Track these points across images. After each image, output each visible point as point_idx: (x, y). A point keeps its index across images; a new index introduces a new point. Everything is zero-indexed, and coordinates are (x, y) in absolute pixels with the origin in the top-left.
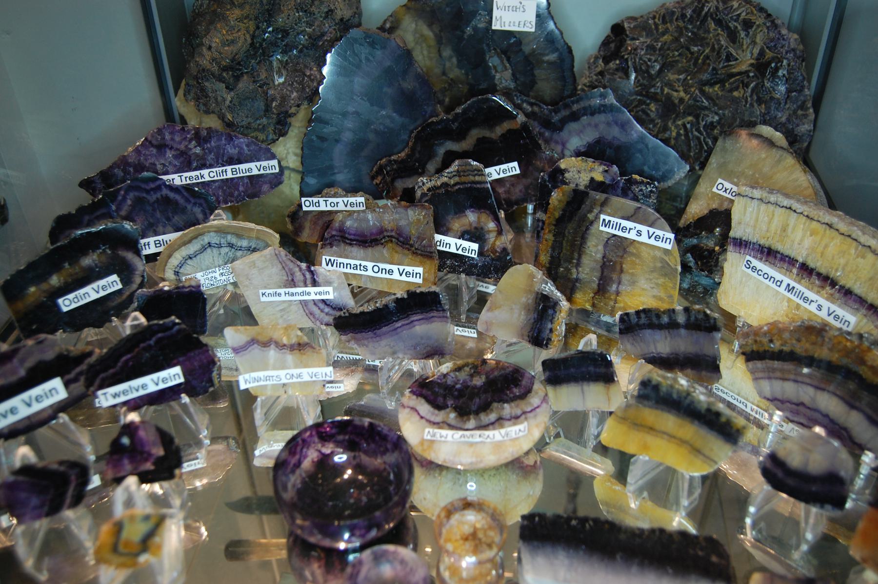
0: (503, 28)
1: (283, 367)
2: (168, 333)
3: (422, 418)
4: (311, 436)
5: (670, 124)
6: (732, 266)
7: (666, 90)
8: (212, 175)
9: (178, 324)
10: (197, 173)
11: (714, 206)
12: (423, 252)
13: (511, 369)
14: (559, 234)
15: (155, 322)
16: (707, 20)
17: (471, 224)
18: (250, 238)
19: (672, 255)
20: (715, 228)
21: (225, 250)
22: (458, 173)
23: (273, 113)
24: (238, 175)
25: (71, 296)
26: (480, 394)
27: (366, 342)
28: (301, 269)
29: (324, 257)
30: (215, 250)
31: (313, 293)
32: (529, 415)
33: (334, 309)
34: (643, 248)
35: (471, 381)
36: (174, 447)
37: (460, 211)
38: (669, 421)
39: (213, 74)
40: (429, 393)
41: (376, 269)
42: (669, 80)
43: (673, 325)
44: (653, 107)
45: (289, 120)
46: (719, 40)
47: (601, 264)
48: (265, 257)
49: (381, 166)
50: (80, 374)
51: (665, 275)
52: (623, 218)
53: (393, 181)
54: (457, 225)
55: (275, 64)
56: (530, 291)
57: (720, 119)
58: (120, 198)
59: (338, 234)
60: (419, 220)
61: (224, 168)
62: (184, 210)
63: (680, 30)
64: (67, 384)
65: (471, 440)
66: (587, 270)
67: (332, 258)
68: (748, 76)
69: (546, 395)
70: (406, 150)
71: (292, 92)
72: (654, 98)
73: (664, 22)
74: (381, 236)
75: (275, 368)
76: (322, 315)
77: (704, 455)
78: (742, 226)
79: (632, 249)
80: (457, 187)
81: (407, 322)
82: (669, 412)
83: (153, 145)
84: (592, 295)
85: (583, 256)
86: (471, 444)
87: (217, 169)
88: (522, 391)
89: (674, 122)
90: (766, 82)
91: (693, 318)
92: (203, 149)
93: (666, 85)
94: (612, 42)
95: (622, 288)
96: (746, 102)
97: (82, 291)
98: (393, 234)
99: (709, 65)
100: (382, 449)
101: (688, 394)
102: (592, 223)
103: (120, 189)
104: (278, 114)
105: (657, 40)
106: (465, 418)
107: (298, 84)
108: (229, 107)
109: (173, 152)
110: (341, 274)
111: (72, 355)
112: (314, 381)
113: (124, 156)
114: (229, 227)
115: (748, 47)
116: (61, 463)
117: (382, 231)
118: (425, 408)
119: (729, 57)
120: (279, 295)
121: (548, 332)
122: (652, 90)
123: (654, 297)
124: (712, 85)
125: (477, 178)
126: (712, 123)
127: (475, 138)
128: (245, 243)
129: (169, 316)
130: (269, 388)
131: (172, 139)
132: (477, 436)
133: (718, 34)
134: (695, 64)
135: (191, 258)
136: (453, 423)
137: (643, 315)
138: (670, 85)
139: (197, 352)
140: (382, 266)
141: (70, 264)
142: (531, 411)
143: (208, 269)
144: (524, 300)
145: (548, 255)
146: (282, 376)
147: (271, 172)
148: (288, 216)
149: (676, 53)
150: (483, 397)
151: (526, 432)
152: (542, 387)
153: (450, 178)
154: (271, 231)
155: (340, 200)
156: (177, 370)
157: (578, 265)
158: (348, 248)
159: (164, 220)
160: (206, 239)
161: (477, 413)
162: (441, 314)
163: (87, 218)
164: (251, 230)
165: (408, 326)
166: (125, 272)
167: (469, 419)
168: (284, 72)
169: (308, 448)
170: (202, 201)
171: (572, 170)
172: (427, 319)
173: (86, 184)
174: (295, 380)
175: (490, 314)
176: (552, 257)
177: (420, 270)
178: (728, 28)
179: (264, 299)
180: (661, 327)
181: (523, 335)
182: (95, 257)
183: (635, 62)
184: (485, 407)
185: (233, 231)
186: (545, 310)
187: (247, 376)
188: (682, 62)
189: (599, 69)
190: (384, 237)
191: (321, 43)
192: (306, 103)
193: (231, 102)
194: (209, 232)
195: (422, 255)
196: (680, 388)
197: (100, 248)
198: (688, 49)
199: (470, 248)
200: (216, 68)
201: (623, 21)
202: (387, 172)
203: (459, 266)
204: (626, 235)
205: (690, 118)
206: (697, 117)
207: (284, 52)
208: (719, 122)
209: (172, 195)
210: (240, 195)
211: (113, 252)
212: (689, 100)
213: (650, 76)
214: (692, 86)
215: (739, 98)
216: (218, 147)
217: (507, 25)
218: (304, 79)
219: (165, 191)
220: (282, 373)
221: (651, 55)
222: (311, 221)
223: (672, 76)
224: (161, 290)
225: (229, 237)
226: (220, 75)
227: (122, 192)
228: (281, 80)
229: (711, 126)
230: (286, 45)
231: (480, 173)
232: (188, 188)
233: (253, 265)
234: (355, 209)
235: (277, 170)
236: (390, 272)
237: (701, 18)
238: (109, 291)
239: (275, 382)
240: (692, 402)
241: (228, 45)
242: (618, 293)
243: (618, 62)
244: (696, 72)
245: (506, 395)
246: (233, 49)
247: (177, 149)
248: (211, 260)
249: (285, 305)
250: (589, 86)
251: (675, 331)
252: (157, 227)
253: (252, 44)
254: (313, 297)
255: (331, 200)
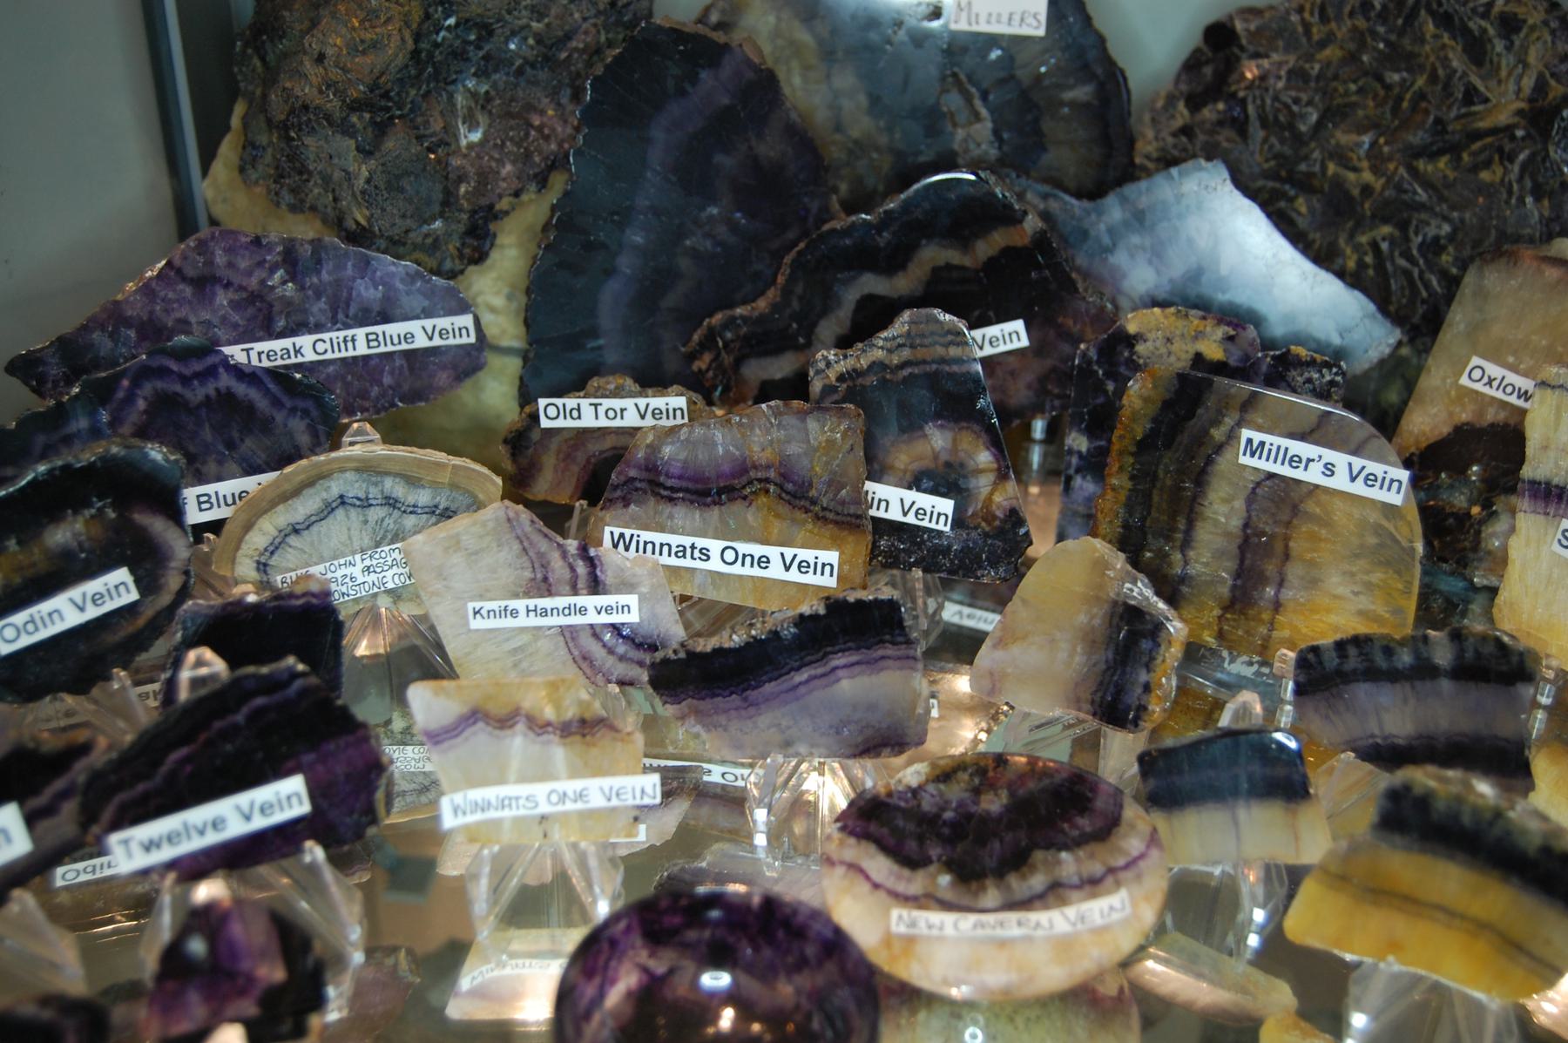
0: (975, 28)
1: (543, 774)
2: (277, 697)
3: (876, 886)
4: (628, 930)
5: (1342, 242)
6: (1527, 544)
7: (1332, 168)
8: (320, 347)
9: (303, 674)
10: (287, 343)
11: (1465, 417)
12: (842, 518)
13: (1064, 775)
14: (1144, 478)
15: (251, 669)
16: (1418, 15)
17: (936, 457)
18: (435, 486)
19: (1402, 517)
20: (1469, 466)
21: (375, 513)
22: (910, 340)
23: (461, 210)
24: (382, 349)
25: (19, 618)
26: (995, 834)
27: (722, 719)
28: (564, 555)
29: (607, 529)
30: (353, 513)
31: (593, 610)
32: (1123, 875)
33: (639, 646)
34: (1338, 503)
35: (976, 803)
36: (310, 962)
37: (911, 425)
38: (1449, 879)
39: (328, 118)
40: (885, 831)
41: (730, 556)
42: (1338, 145)
43: (1424, 670)
44: (1301, 204)
45: (492, 227)
46: (1446, 58)
47: (1239, 541)
48: (484, 525)
49: (711, 329)
50: (64, 795)
51: (1387, 564)
52: (1292, 436)
53: (738, 362)
54: (904, 457)
55: (460, 100)
56: (1098, 598)
57: (1455, 231)
58: (120, 394)
59: (644, 475)
60: (831, 443)
61: (350, 332)
62: (266, 426)
63: (1359, 37)
64: (31, 820)
65: (999, 932)
66: (1207, 555)
67: (628, 532)
68: (1513, 138)
69: (1155, 830)
70: (771, 293)
71: (501, 162)
72: (1306, 185)
73: (1324, 19)
74: (744, 480)
75: (523, 779)
76: (610, 661)
77: (1531, 955)
78: (1552, 454)
79: (1311, 506)
80: (906, 372)
81: (820, 671)
82: (1451, 857)
83: (184, 279)
84: (1217, 612)
85: (1199, 524)
86: (1003, 943)
87: (333, 335)
88: (1099, 823)
89: (1351, 236)
90: (1551, 149)
91: (1469, 655)
92: (302, 288)
93: (1331, 156)
94: (1207, 62)
95: (1287, 594)
96: (1510, 192)
97: (45, 607)
98: (772, 474)
99: (1427, 112)
100: (790, 960)
101: (1498, 814)
102: (1219, 448)
103: (122, 374)
104: (473, 212)
105: (1310, 58)
106: (974, 885)
107: (518, 145)
108: (363, 192)
109: (231, 295)
110: (665, 564)
111: (45, 749)
112: (614, 810)
113: (116, 303)
114: (388, 458)
115: (1510, 74)
116: (47, 1000)
117: (743, 468)
118: (879, 866)
119: (1471, 96)
120: (514, 613)
121: (1139, 690)
122: (1303, 167)
123: (1361, 613)
124: (1433, 156)
125: (954, 351)
126: (1437, 239)
127: (927, 268)
128: (423, 497)
129: (280, 656)
130: (507, 826)
131: (231, 265)
132: (1012, 924)
133: (1444, 46)
134: (1396, 110)
135: (296, 531)
136: (948, 896)
137: (1352, 651)
138: (1341, 157)
139: (342, 742)
140: (743, 548)
141: (19, 543)
142: (1127, 866)
143: (335, 558)
144: (1082, 618)
145: (1118, 522)
146: (540, 797)
147: (458, 341)
148: (506, 441)
149: (1353, 87)
150: (1009, 837)
151: (1128, 910)
152: (1141, 811)
153: (890, 351)
154: (485, 470)
155: (628, 403)
156: (295, 784)
157: (1186, 545)
158: (667, 509)
159: (221, 448)
160: (335, 487)
161: (1000, 873)
162: (902, 651)
163: (41, 440)
164: (439, 465)
165: (824, 681)
166: (145, 560)
167: (983, 889)
168: (482, 119)
169: (620, 960)
170: (309, 404)
171: (1151, 336)
172: (872, 664)
173: (25, 368)
174: (569, 806)
175: (999, 654)
176: (1126, 526)
177: (832, 557)
178: (1466, 31)
179: (477, 624)
180: (1393, 676)
181: (1078, 700)
182: (79, 526)
183: (1263, 105)
184: (1017, 861)
185: (397, 468)
186: (1134, 637)
187: (458, 798)
188: (1365, 107)
189: (1178, 123)
190: (750, 483)
191: (563, 55)
192: (533, 187)
193: (368, 181)
194: (343, 470)
195: (836, 523)
196: (1480, 801)
197: (89, 505)
198: (1380, 78)
199: (935, 511)
200: (337, 103)
201: (1231, 18)
202: (726, 345)
203: (908, 552)
204: (1298, 474)
205: (1386, 230)
206: (1403, 226)
207: (481, 74)
208: (1451, 238)
209: (241, 389)
210: (383, 395)
211: (120, 516)
212: (1384, 188)
213: (1298, 140)
214: (1390, 159)
215: (1492, 185)
216: (338, 283)
217: (983, 19)
218: (527, 135)
219: (225, 381)
220: (540, 790)
221: (1299, 90)
222: (559, 452)
223: (1343, 137)
224: (239, 603)
225: (388, 483)
226: (344, 119)
227: (126, 383)
228: (476, 137)
229: (1434, 247)
230: (487, 58)
231: (959, 339)
232: (280, 376)
233: (455, 544)
234: (665, 422)
235: (472, 339)
236: (764, 562)
237: (1406, 11)
238: (109, 606)
239: (522, 812)
240: (1508, 833)
241: (364, 53)
242: (1277, 606)
243: (1221, 106)
244: (1396, 129)
245: (1063, 832)
246: (366, 63)
247: (241, 288)
248: (344, 538)
249: (526, 638)
250: (1158, 160)
251: (1428, 684)
252: (204, 463)
253: (415, 53)
254: (593, 618)
255: (607, 403)
